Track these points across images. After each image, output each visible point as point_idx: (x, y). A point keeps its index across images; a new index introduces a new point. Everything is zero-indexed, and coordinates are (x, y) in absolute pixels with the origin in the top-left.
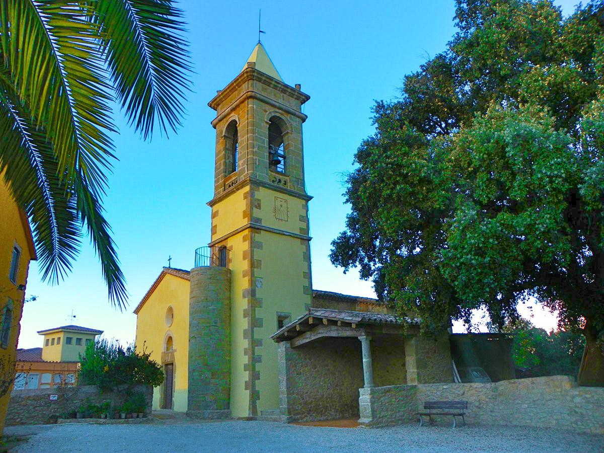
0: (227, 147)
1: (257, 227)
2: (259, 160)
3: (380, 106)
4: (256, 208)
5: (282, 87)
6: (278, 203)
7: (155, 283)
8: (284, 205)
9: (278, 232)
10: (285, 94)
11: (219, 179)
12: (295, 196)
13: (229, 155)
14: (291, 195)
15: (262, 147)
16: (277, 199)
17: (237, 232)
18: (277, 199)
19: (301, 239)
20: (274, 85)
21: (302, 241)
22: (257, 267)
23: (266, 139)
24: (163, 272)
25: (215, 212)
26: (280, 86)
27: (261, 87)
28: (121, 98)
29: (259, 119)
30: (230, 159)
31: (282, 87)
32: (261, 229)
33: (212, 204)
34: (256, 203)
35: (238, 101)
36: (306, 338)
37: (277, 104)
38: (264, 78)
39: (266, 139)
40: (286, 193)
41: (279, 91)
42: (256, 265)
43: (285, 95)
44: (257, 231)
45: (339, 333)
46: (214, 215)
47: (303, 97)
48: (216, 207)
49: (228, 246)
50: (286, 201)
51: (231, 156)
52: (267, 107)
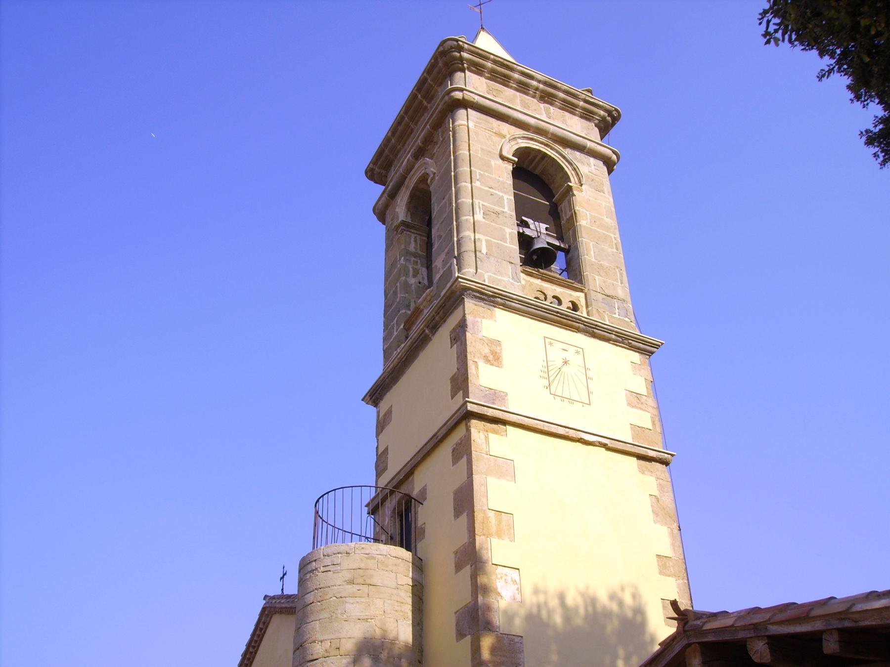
0: (412, 248)
1: (490, 413)
2: (487, 241)
3: (866, 144)
4: (487, 360)
5: (541, 86)
6: (556, 355)
7: (249, 645)
8: (575, 360)
9: (561, 431)
10: (551, 104)
11: (393, 327)
12: (607, 340)
13: (419, 266)
14: (594, 335)
15: (497, 214)
16: (551, 344)
17: (435, 441)
18: (551, 344)
19: (641, 457)
20: (520, 83)
21: (642, 462)
22: (499, 535)
23: (506, 197)
24: (264, 609)
25: (385, 415)
26: (534, 83)
27: (485, 85)
28: (338, 559)
29: (482, 149)
30: (420, 277)
31: (541, 86)
32: (504, 422)
33: (375, 395)
34: (486, 350)
35: (428, 126)
36: (436, 224)
37: (532, 121)
38: (489, 65)
39: (506, 197)
40: (578, 330)
41: (534, 97)
42: (494, 529)
43: (552, 108)
44: (494, 426)
45: (646, 400)
46: (381, 425)
47: (602, 113)
48: (389, 399)
49: (415, 493)
50: (580, 351)
51: (424, 271)
52: (507, 129)
